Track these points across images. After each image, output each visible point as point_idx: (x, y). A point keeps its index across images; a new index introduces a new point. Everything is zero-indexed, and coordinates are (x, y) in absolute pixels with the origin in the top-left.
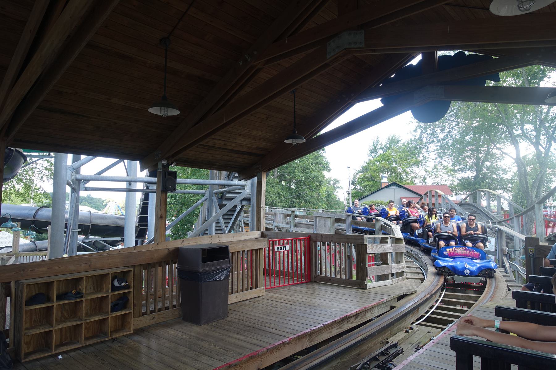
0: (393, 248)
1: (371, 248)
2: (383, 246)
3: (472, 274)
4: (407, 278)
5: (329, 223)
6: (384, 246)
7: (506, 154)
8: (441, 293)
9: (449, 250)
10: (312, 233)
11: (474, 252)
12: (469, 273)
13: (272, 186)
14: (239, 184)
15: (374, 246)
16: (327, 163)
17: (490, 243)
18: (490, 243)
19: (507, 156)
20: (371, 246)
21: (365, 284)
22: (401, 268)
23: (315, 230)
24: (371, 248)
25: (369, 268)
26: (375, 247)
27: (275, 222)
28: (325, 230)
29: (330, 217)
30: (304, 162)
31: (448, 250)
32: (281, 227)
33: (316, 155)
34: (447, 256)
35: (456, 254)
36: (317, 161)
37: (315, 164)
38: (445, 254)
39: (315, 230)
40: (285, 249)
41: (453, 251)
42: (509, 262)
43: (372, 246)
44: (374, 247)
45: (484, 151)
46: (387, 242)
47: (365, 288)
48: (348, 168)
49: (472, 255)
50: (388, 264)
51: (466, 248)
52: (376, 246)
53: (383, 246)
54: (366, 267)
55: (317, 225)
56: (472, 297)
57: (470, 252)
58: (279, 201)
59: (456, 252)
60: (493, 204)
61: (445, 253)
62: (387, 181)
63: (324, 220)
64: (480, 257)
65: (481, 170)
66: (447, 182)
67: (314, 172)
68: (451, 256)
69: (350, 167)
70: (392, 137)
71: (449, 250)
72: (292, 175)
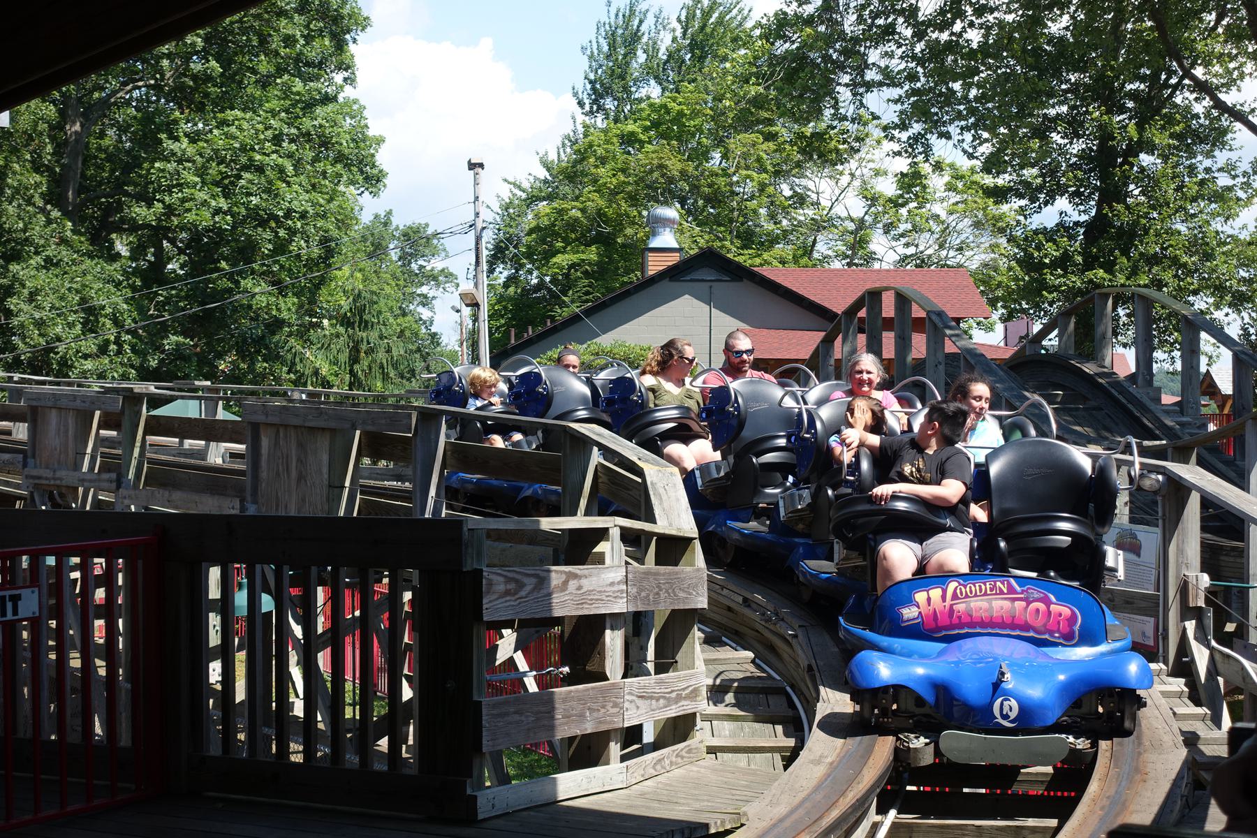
0: (633, 590)
1: (507, 593)
2: (576, 576)
3: (1027, 721)
4: (712, 750)
5: (325, 458)
6: (584, 582)
7: (1238, 115)
8: (878, 818)
9: (929, 599)
10: (235, 512)
11: (1047, 602)
12: (1013, 715)
13: (48, 260)
14: (564, 332)
15: (526, 580)
16: (360, 138)
17: (1139, 555)
18: (1139, 555)
19: (1238, 125)
20: (506, 583)
21: (469, 791)
22: (679, 698)
23: (249, 498)
24: (507, 593)
25: (495, 706)
26: (528, 588)
27: (34, 457)
28: (303, 500)
29: (332, 424)
30: (233, 129)
31: (920, 597)
32: (68, 487)
33: (298, 93)
34: (918, 631)
35: (959, 617)
36: (307, 124)
37: (292, 141)
38: (906, 617)
39: (249, 498)
40: (15, 612)
41: (948, 603)
42: (1214, 643)
43: (509, 580)
44: (521, 585)
45: (1134, 95)
46: (600, 559)
47: (466, 812)
48: (472, 166)
49: (1039, 622)
50: (607, 679)
51: (1011, 590)
52: (534, 580)
53: (576, 576)
54: (476, 698)
55: (264, 475)
56: (1025, 833)
57: (1029, 603)
58: (90, 345)
59: (960, 607)
60: (1166, 362)
61: (909, 613)
62: (676, 245)
63: (301, 446)
64: (1077, 628)
65: (1121, 196)
66: (968, 254)
67: (288, 184)
68: (939, 629)
69: (481, 165)
70: (707, 14)
71: (929, 599)
72: (163, 202)
